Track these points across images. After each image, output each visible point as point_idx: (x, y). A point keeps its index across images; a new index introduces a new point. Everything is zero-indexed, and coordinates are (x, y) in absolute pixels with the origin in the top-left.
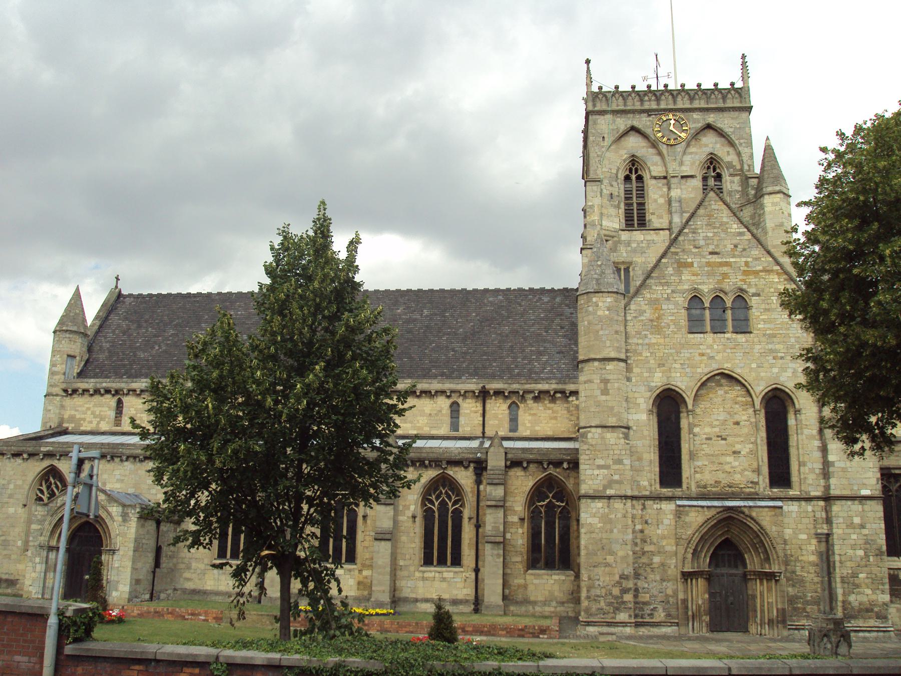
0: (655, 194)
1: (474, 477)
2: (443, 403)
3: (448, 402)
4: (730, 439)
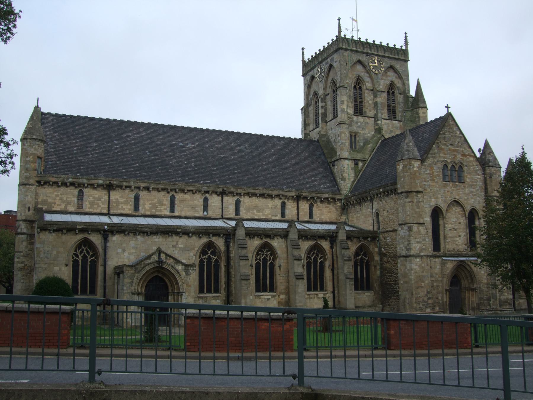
0: (368, 98)
1: (330, 245)
2: (278, 202)
4: (458, 230)
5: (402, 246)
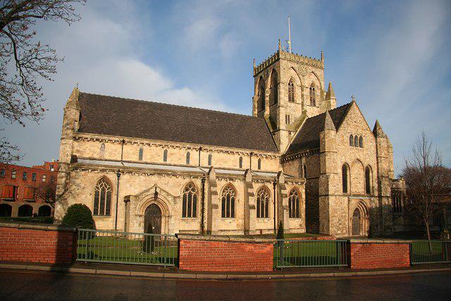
3: (239, 157)
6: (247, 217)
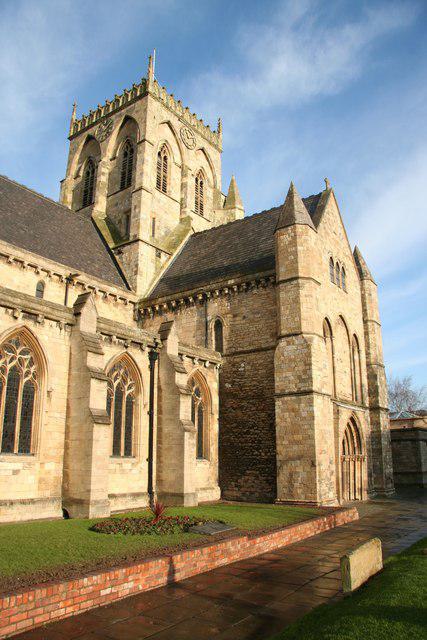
5: (289, 374)
6: (77, 452)
